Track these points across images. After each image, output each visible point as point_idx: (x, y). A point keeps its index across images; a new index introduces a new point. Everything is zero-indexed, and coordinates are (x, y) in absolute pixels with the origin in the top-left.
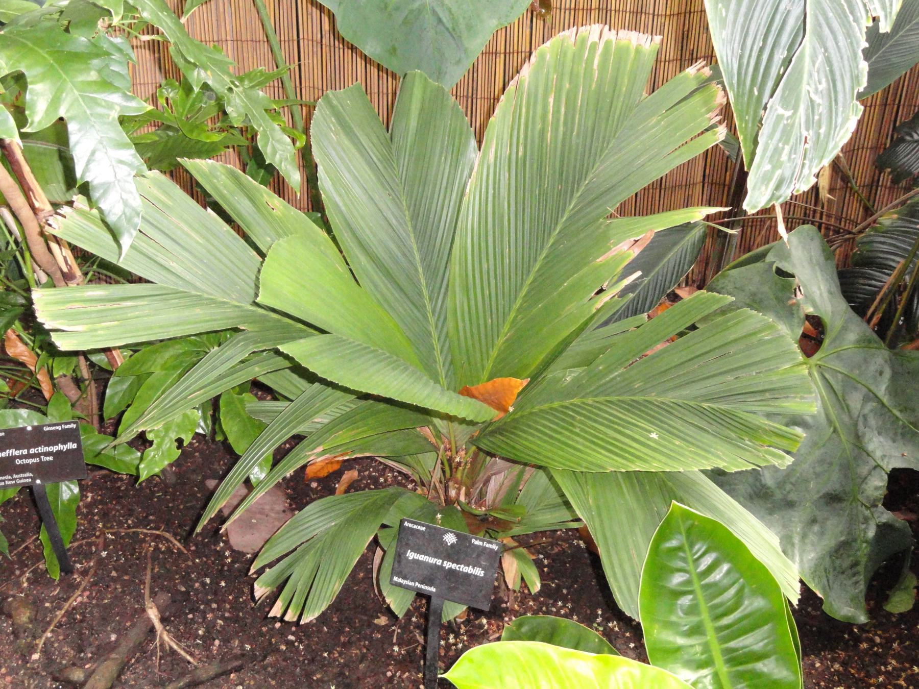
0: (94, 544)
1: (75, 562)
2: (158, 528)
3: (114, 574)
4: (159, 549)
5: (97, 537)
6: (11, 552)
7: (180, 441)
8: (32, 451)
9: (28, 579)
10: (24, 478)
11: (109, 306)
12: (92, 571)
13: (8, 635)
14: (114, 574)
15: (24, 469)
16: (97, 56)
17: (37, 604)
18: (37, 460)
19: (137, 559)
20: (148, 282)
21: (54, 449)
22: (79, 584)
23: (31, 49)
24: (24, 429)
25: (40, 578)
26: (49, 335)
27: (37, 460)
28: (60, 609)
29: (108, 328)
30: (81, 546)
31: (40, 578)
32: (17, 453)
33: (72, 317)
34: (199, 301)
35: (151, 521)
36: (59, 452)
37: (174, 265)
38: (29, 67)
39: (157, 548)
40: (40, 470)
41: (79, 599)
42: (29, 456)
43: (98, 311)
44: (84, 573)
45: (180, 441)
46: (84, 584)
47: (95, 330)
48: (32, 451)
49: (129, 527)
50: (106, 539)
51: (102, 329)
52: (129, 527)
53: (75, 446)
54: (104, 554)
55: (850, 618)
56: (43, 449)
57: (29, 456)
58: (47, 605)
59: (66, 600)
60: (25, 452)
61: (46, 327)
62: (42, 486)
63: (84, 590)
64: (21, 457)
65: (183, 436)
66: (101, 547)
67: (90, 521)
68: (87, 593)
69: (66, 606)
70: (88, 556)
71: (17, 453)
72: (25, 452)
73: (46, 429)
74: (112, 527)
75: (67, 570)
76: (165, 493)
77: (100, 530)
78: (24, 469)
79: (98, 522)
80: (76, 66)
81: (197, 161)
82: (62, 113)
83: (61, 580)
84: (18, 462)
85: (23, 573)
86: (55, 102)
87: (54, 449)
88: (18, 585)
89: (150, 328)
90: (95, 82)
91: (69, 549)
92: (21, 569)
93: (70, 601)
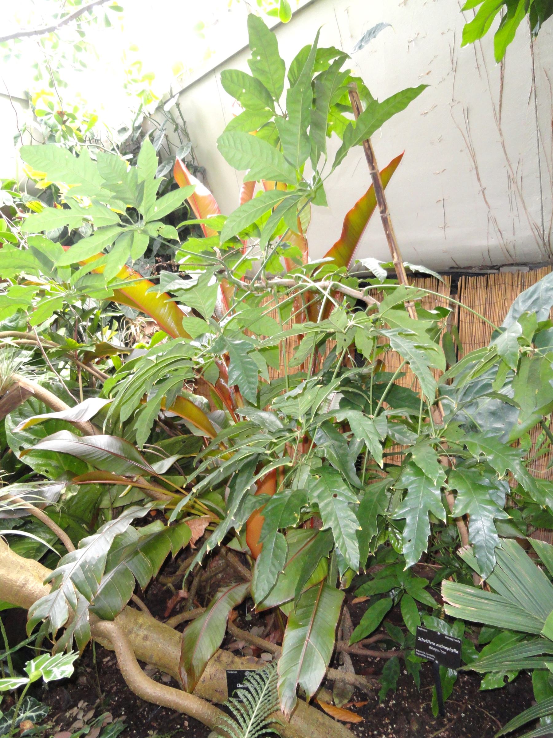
0: (459, 706)
1: (448, 711)
2: (495, 716)
3: (464, 729)
4: (492, 729)
5: (463, 703)
6: (421, 688)
7: (506, 677)
8: (437, 645)
9: (423, 708)
10: (431, 657)
11: (475, 599)
12: (453, 722)
13: (406, 732)
14: (464, 729)
15: (432, 652)
16: (491, 488)
17: (422, 724)
18: (438, 651)
19: (479, 728)
20: (498, 594)
21: (448, 649)
22: (446, 725)
23: (464, 480)
24: (436, 633)
25: (428, 710)
26: (443, 605)
27: (438, 651)
28: (432, 733)
29: (471, 610)
30: (453, 704)
31: (428, 710)
32: (431, 643)
33: (457, 599)
34: (521, 612)
35: (494, 710)
36: (449, 652)
37: (513, 589)
38: (459, 489)
39: (491, 728)
40: (438, 656)
41: (442, 734)
42: (435, 647)
43: (468, 600)
44: (450, 720)
45: (506, 677)
46: (447, 727)
47: (465, 610)
48: (437, 645)
49: (481, 706)
50: (467, 706)
51: (468, 610)
52: (481, 706)
53: (457, 652)
54: (463, 715)
55: (109, 632)
56: (442, 646)
57: (435, 647)
58: (427, 727)
59: (437, 730)
60: (434, 644)
61: (444, 599)
62: (438, 665)
63: (447, 730)
64: (432, 646)
65: (509, 675)
66: (463, 710)
67: (463, 692)
68: (447, 733)
69: (435, 734)
70: (455, 711)
71: (431, 643)
72: (434, 644)
73: (446, 637)
74: (472, 701)
75: (442, 714)
76: (507, 697)
77: (466, 700)
78: (432, 652)
79: (466, 694)
80: (481, 492)
81: (538, 541)
82: (468, 511)
83: (438, 717)
84: (430, 648)
85: (422, 703)
86: (466, 506)
87: (448, 649)
88: (419, 708)
89: (492, 618)
90: (487, 500)
91: (446, 703)
92: (422, 700)
93: (439, 732)
